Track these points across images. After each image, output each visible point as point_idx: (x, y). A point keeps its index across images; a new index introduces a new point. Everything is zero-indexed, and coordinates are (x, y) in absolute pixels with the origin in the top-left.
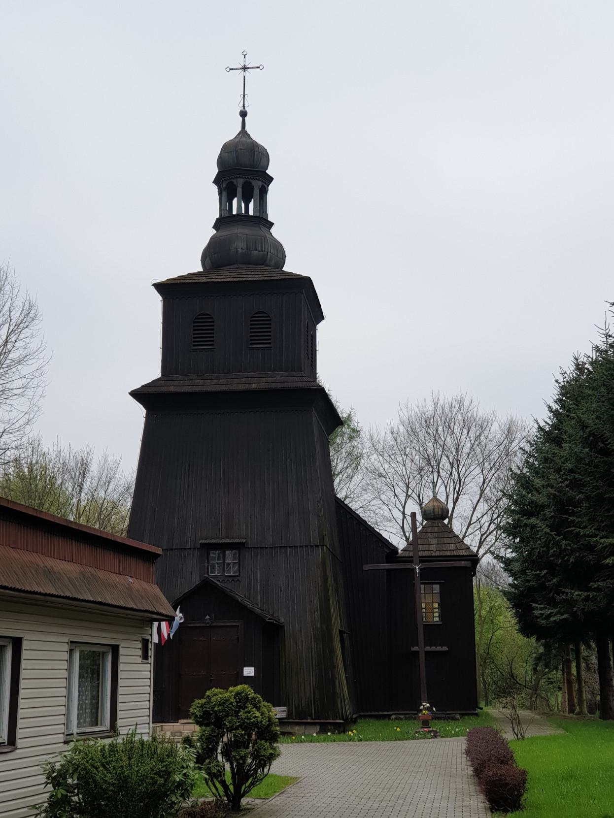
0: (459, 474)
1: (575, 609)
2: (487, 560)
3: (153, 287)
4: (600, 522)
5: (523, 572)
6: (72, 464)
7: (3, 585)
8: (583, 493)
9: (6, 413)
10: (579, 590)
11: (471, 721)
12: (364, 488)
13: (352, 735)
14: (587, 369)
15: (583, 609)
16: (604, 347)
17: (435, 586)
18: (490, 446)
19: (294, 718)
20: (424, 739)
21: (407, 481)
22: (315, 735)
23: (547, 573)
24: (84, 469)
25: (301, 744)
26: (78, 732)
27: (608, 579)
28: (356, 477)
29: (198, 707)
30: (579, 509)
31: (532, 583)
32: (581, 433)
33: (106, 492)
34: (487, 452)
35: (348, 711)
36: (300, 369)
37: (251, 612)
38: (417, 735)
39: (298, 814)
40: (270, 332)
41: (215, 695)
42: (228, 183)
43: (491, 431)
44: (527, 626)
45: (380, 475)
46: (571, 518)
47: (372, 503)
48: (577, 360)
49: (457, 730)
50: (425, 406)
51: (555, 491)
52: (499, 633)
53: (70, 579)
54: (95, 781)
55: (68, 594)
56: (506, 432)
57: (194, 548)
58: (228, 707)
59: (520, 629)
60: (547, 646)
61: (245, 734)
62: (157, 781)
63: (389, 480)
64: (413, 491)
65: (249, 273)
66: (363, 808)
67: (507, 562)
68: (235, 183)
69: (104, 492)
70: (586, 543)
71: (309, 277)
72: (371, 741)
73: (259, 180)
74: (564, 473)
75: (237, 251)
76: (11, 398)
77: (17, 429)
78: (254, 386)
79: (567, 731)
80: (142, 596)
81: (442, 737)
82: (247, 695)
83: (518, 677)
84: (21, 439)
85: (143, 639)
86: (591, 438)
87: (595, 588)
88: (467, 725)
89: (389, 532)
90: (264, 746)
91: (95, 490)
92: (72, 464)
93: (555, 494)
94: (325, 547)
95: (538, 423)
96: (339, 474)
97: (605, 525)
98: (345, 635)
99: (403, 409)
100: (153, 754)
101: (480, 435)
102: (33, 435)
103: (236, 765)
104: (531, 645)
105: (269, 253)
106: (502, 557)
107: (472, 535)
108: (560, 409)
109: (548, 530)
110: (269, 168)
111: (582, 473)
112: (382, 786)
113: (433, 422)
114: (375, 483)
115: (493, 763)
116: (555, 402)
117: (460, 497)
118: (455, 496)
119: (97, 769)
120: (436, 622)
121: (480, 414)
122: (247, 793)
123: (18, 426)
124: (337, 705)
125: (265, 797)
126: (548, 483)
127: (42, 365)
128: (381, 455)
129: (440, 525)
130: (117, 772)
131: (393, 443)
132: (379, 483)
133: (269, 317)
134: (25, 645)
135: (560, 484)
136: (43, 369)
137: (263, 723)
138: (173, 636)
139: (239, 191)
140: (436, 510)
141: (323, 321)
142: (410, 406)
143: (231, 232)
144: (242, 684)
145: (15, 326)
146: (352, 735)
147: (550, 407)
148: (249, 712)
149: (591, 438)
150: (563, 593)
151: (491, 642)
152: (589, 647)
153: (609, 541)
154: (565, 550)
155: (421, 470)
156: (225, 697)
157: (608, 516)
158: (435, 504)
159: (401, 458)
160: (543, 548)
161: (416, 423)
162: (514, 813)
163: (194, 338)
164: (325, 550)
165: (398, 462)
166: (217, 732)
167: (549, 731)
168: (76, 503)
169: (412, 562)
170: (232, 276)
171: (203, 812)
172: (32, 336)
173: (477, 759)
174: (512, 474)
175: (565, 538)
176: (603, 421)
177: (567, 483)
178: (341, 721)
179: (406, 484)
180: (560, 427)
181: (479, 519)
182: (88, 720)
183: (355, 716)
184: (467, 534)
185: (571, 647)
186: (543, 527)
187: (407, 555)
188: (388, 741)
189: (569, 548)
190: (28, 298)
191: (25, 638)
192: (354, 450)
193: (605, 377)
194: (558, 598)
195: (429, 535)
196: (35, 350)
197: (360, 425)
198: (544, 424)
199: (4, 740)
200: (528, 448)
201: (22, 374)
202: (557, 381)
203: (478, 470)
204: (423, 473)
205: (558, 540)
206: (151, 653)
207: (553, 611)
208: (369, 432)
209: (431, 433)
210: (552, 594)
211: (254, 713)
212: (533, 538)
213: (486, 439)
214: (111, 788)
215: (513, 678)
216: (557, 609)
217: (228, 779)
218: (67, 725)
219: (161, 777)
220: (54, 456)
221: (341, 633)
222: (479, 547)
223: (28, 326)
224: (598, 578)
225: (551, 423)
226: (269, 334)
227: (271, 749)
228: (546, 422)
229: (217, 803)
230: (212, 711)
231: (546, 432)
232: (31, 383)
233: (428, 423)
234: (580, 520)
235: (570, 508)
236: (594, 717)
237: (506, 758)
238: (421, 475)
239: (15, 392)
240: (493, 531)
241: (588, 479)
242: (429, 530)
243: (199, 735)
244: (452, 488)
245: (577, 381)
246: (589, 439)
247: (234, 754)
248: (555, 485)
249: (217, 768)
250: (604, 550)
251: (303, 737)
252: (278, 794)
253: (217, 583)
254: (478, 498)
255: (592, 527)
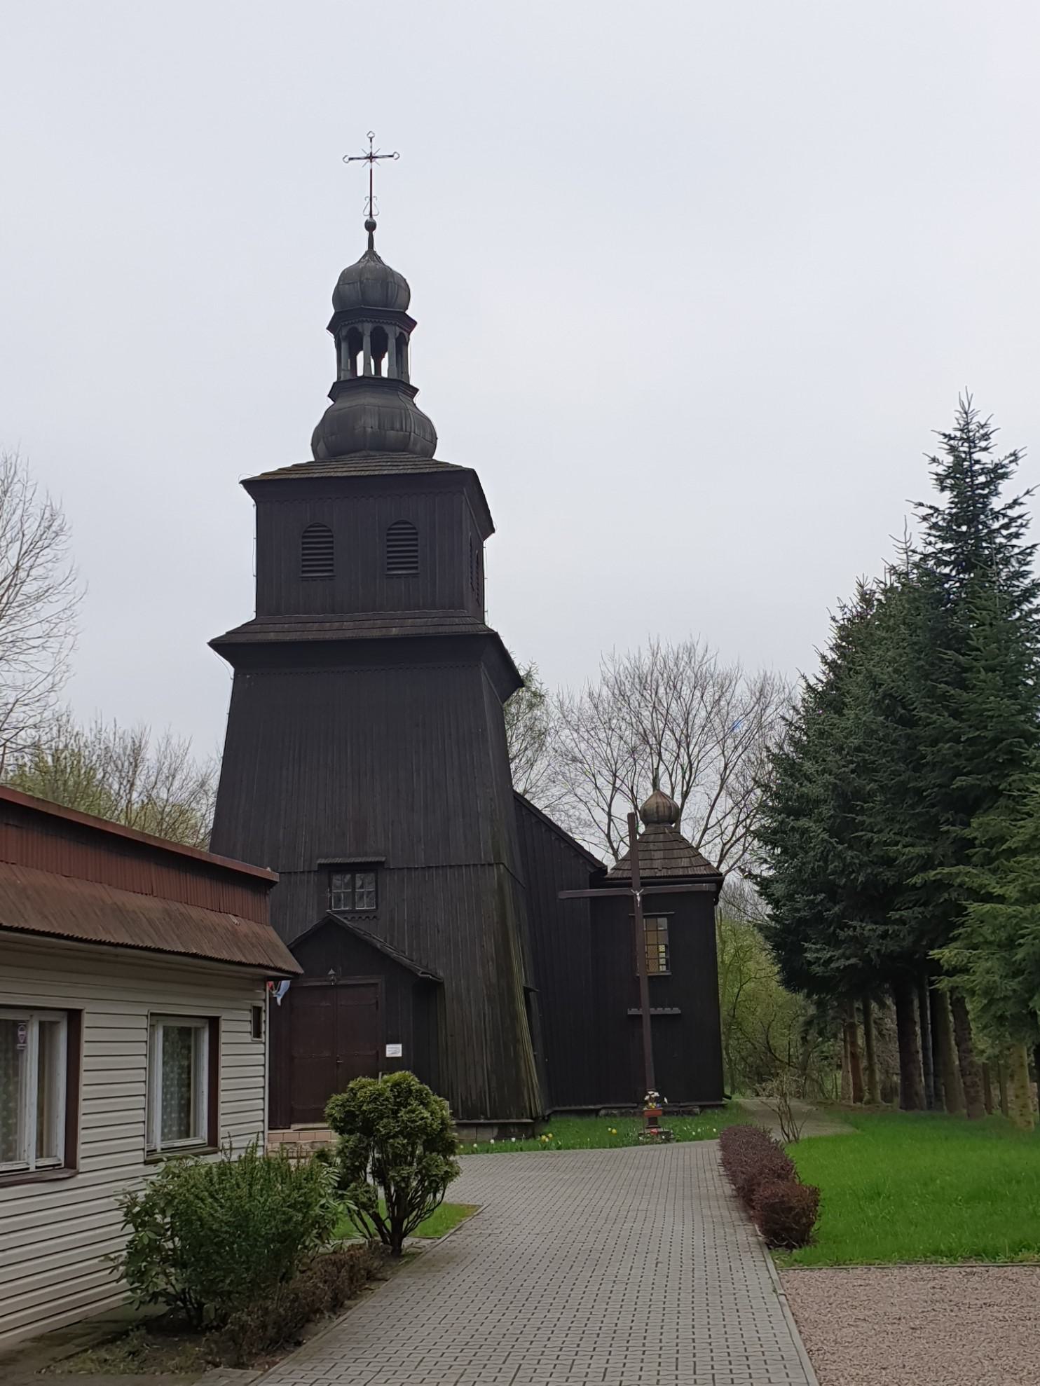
0: (689, 757)
1: (867, 950)
2: (732, 879)
3: (241, 485)
4: (903, 823)
5: (790, 897)
6: (119, 750)
7: (31, 928)
8: (876, 781)
9: (18, 675)
10: (872, 922)
11: (716, 1117)
12: (551, 778)
13: (547, 1140)
14: (878, 600)
15: (878, 951)
16: (903, 568)
17: (660, 920)
18: (735, 715)
19: (461, 1117)
20: (651, 1144)
21: (614, 767)
22: (492, 1141)
23: (825, 897)
24: (136, 754)
25: (473, 1156)
26: (163, 1146)
27: (914, 906)
28: (539, 762)
29: (337, 1106)
30: (872, 804)
31: (802, 913)
32: (872, 694)
33: (169, 790)
34: (729, 724)
35: (539, 1106)
36: (462, 607)
37: (396, 963)
38: (641, 1138)
39: (487, 1260)
40: (416, 551)
41: (362, 1088)
42: (350, 329)
43: (736, 693)
44: (795, 977)
45: (574, 759)
46: (859, 818)
47: (564, 800)
48: (862, 587)
49: (699, 1130)
50: (640, 657)
51: (835, 778)
52: (749, 986)
53: (150, 922)
54: (200, 1219)
55: (149, 944)
56: (758, 694)
57: (309, 872)
58: (382, 1105)
59: (784, 980)
60: (820, 1004)
61: (408, 1144)
62: (291, 1218)
63: (586, 766)
64: (623, 782)
65: (384, 464)
66: (582, 1249)
67: (765, 886)
68: (360, 330)
69: (166, 790)
70: (882, 853)
71: (472, 473)
72: (575, 1148)
73: (395, 324)
74: (848, 753)
75: (365, 432)
76: (26, 652)
77: (36, 699)
78: (394, 631)
79: (858, 1128)
80: (252, 944)
81: (678, 1141)
82: (409, 1085)
83: (778, 1051)
84: (41, 713)
85: (254, 1007)
86: (887, 701)
87: (896, 919)
88: (716, 1122)
89: (588, 842)
90: (436, 1161)
91: (153, 788)
92: (119, 750)
93: (835, 783)
94: (501, 866)
95: (806, 681)
96: (515, 758)
97: (910, 828)
98: (531, 994)
99: (607, 662)
100: (286, 1175)
101: (719, 700)
102: (61, 707)
103: (395, 1191)
104: (800, 1004)
105: (412, 434)
106: (756, 877)
107: (710, 844)
108: (839, 659)
109: (826, 836)
110: (410, 307)
111: (874, 752)
112: (604, 1215)
113: (651, 681)
114: (567, 772)
115: (766, 1177)
116: (831, 649)
117: (692, 789)
118: (685, 789)
119: (202, 1200)
120: (663, 972)
121: (720, 667)
122: (411, 1230)
123: (38, 694)
124: (523, 1098)
125: (436, 1235)
126: (824, 768)
127: (72, 603)
128: (576, 731)
129: (667, 831)
130: (232, 1205)
131: (592, 712)
132: (572, 771)
133: (414, 528)
134: (86, 1020)
135: (843, 769)
136: (73, 608)
137: (434, 1127)
138: (282, 1000)
139: (367, 341)
140: (661, 809)
141: (493, 535)
142: (616, 657)
143: (354, 403)
144: (401, 1070)
145: (31, 544)
146: (547, 1140)
147: (823, 657)
148: (413, 1111)
149: (887, 701)
150: (849, 927)
151: (739, 1000)
152: (882, 1005)
153: (917, 851)
154: (852, 864)
155: (633, 751)
156: (378, 1090)
157: (914, 814)
158: (659, 800)
159: (604, 735)
160: (819, 861)
161: (627, 683)
162: (803, 1249)
163: (304, 560)
164: (502, 871)
165: (600, 740)
166: (366, 1142)
167: (831, 1129)
168: (124, 807)
169: (630, 885)
170: (358, 469)
171: (352, 1261)
172: (56, 560)
173: (743, 1173)
174: (769, 756)
175: (850, 847)
176: (904, 676)
177: (852, 766)
178: (530, 1121)
179: (612, 771)
180: (840, 685)
181: (719, 821)
182: (175, 1129)
183: (548, 1112)
184: (703, 843)
185: (856, 1005)
186: (820, 831)
187: (619, 876)
188: (599, 1148)
189: (857, 861)
190: (49, 504)
191: (86, 1011)
192: (537, 723)
193: (905, 612)
194: (842, 935)
195: (651, 846)
196: (61, 581)
197: (544, 687)
198: (816, 681)
199: (60, 1160)
200: (789, 714)
201: (43, 615)
202: (833, 619)
203: (717, 751)
204: (636, 756)
205: (841, 850)
206: (265, 1028)
207: (833, 954)
208: (558, 696)
209: (648, 697)
210: (832, 928)
211: (421, 1113)
212: (802, 848)
213: (728, 704)
214: (226, 1228)
215: (770, 1051)
216: (841, 951)
217: (383, 1212)
218: (147, 1136)
219: (299, 1211)
220: (91, 738)
221: (527, 991)
222: (720, 862)
223: (50, 544)
224: (899, 905)
225: (825, 680)
226: (415, 554)
227: (447, 1164)
228: (817, 679)
229: (370, 1246)
230: (359, 1110)
231: (818, 693)
232: (55, 630)
233: (643, 682)
234: (872, 820)
235: (858, 803)
236: (892, 1107)
237: (785, 1171)
238: (634, 759)
239: (32, 643)
240: (741, 837)
241: (884, 760)
242: (652, 838)
243: (340, 1147)
244: (680, 777)
245: (862, 618)
246: (883, 702)
247: (392, 1173)
248: (835, 770)
249: (368, 1195)
250: (909, 863)
251: (475, 1145)
252: (452, 1231)
253: (345, 921)
254: (717, 791)
255: (891, 830)
